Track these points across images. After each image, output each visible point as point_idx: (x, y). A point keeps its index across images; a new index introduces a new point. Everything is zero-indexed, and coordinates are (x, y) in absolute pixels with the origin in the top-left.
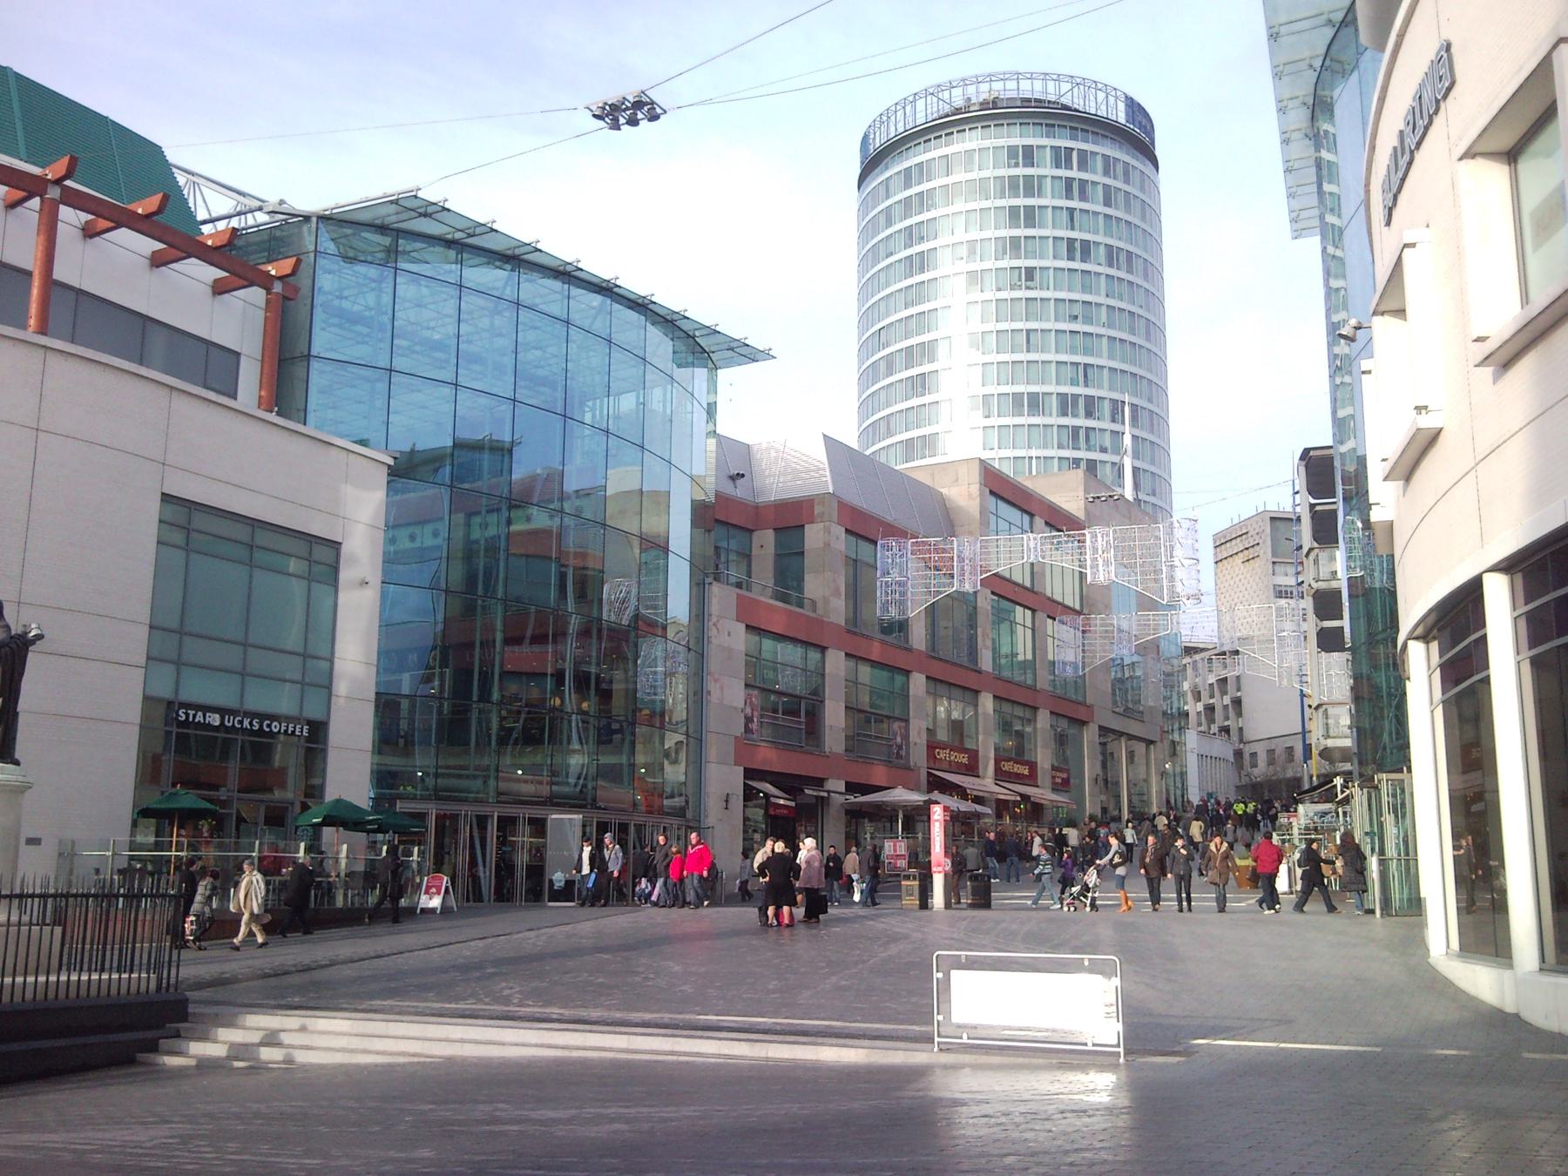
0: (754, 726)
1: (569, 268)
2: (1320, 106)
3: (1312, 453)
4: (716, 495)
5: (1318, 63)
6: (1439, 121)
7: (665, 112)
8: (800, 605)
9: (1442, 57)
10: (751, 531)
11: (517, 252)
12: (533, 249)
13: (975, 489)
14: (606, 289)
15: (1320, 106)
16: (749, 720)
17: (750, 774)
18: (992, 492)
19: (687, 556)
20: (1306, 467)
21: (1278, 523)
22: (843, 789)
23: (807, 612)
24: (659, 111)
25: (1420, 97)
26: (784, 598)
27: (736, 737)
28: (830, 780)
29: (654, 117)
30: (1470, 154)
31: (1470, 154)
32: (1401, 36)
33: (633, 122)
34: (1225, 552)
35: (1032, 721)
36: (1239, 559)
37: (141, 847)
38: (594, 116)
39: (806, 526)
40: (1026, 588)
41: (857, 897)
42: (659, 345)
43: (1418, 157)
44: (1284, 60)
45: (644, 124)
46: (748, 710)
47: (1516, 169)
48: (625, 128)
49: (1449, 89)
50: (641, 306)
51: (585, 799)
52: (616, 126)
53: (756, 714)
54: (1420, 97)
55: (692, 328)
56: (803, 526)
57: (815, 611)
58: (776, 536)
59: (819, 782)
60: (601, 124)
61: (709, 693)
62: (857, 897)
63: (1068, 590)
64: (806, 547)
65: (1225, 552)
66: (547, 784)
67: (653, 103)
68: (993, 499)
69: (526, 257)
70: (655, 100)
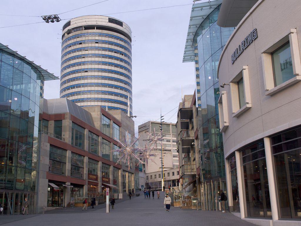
0: (51, 169)
1: (14, 53)
2: (196, 34)
3: (182, 109)
4: (43, 113)
5: (198, 26)
6: (252, 45)
7: (61, 20)
8: (61, 139)
9: (254, 32)
10: (48, 121)
11: (2, 48)
12: (7, 48)
13: (99, 113)
14: (23, 59)
15: (196, 34)
16: (50, 168)
17: (50, 181)
18: (103, 114)
19: (35, 126)
20: (180, 112)
21: (153, 124)
22: (70, 185)
23: (62, 141)
24: (59, 20)
25: (247, 39)
26: (57, 137)
27: (47, 172)
28: (67, 183)
29: (58, 21)
30: (264, 52)
31: (264, 52)
32: (241, 26)
33: (53, 22)
34: (141, 130)
35: (109, 168)
36: (144, 132)
37: (92, 179)
38: (43, 19)
39: (63, 120)
40: (109, 137)
41: (260, 182)
42: (34, 75)
43: (245, 51)
44: (192, 24)
45: (55, 22)
46: (49, 165)
47: (273, 56)
48: (50, 23)
49: (256, 38)
50: (30, 64)
51: (12, 188)
52: (48, 22)
53: (51, 166)
54: (247, 39)
55: (41, 70)
56: (62, 120)
57: (64, 141)
58: (55, 122)
59: (65, 183)
60: (44, 21)
61: (41, 161)
62: (260, 182)
63: (117, 138)
64: (63, 125)
65: (141, 130)
66: (4, 183)
67: (58, 17)
68: (103, 116)
69: (3, 49)
70: (59, 17)
